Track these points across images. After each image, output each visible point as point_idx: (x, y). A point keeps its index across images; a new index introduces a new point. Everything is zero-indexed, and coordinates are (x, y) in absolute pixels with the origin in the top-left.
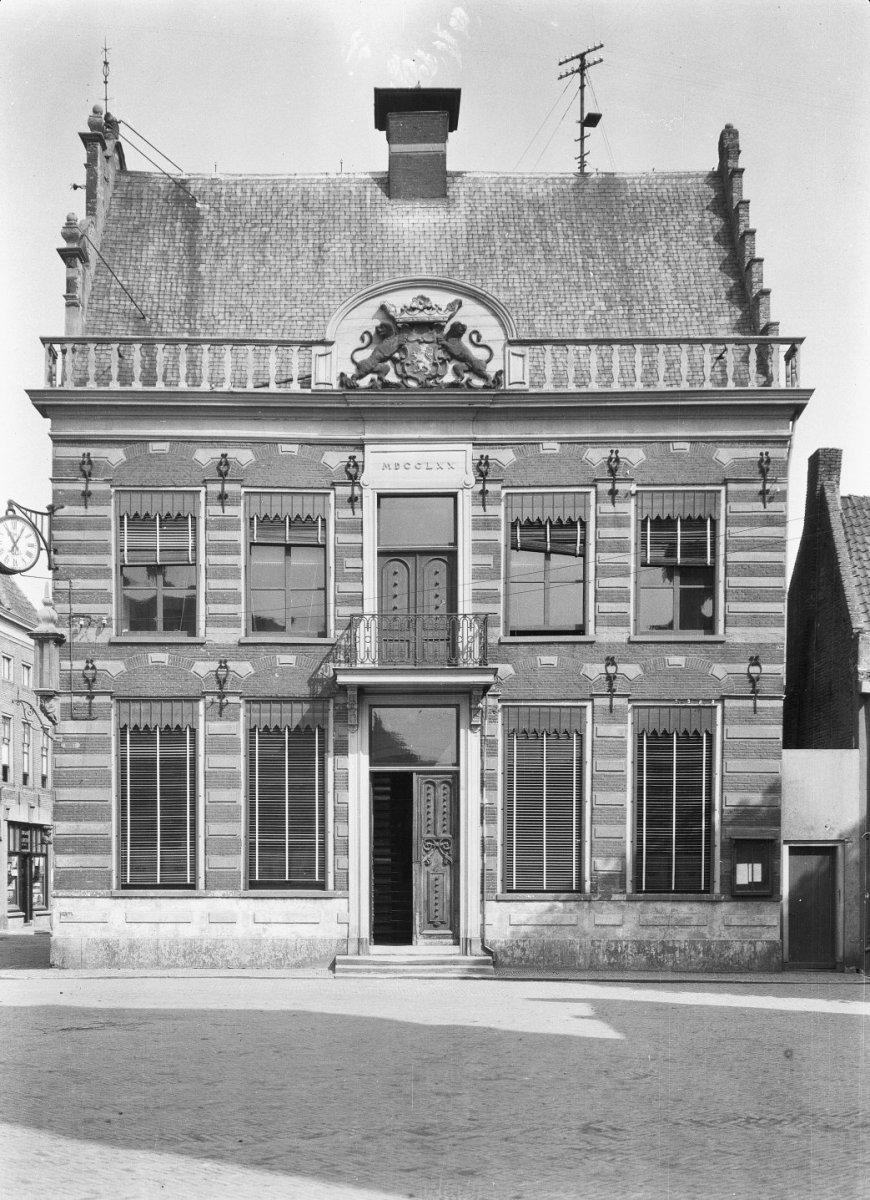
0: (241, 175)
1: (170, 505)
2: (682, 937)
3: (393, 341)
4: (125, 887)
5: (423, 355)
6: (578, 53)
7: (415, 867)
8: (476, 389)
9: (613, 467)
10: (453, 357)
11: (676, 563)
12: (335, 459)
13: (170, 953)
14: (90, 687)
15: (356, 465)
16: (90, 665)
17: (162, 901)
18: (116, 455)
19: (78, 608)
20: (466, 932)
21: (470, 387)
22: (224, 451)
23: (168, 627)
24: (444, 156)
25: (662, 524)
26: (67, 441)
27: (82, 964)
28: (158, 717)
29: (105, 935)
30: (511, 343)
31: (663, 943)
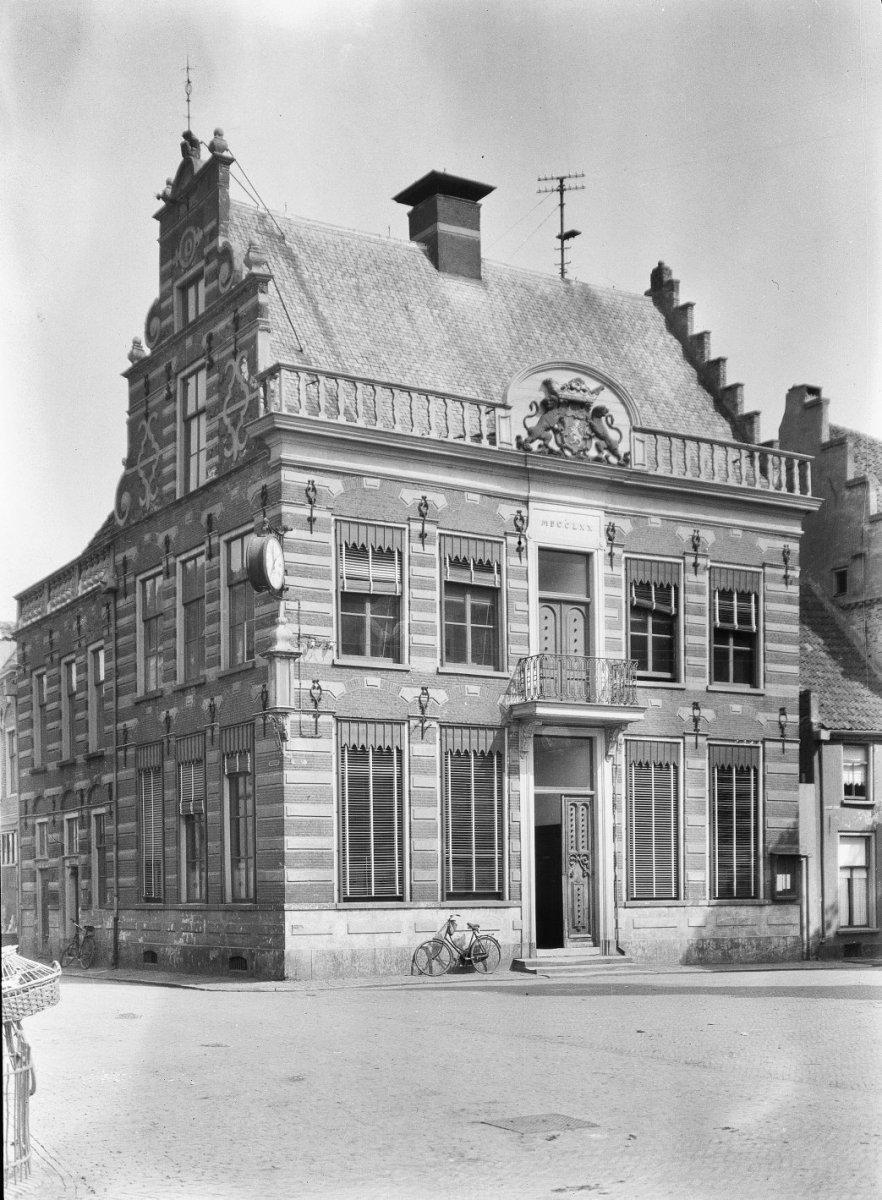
0: (308, 220)
1: (384, 540)
2: (742, 935)
3: (555, 415)
4: (347, 900)
5: (576, 430)
6: (559, 176)
7: (564, 878)
8: (614, 465)
9: (696, 542)
10: (598, 435)
11: (751, 630)
12: (507, 511)
13: (385, 962)
14: (316, 706)
15: (522, 519)
16: (316, 685)
17: (377, 912)
18: (335, 486)
19: (306, 629)
20: (605, 935)
21: (609, 463)
22: (424, 494)
23: (375, 653)
24: (479, 242)
25: (726, 595)
26: (294, 466)
27: (312, 976)
28: (373, 737)
29: (331, 947)
30: (635, 430)
31: (731, 940)
